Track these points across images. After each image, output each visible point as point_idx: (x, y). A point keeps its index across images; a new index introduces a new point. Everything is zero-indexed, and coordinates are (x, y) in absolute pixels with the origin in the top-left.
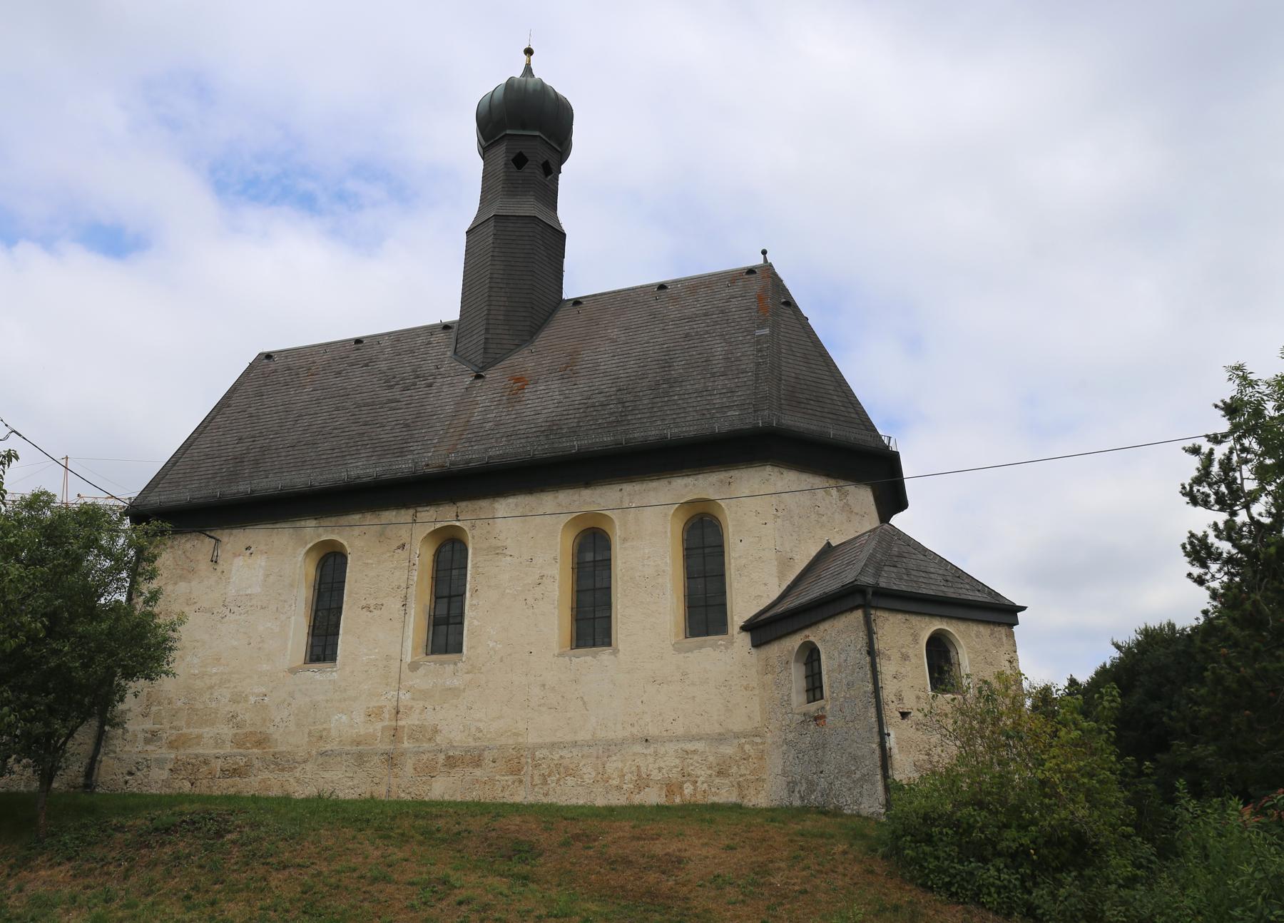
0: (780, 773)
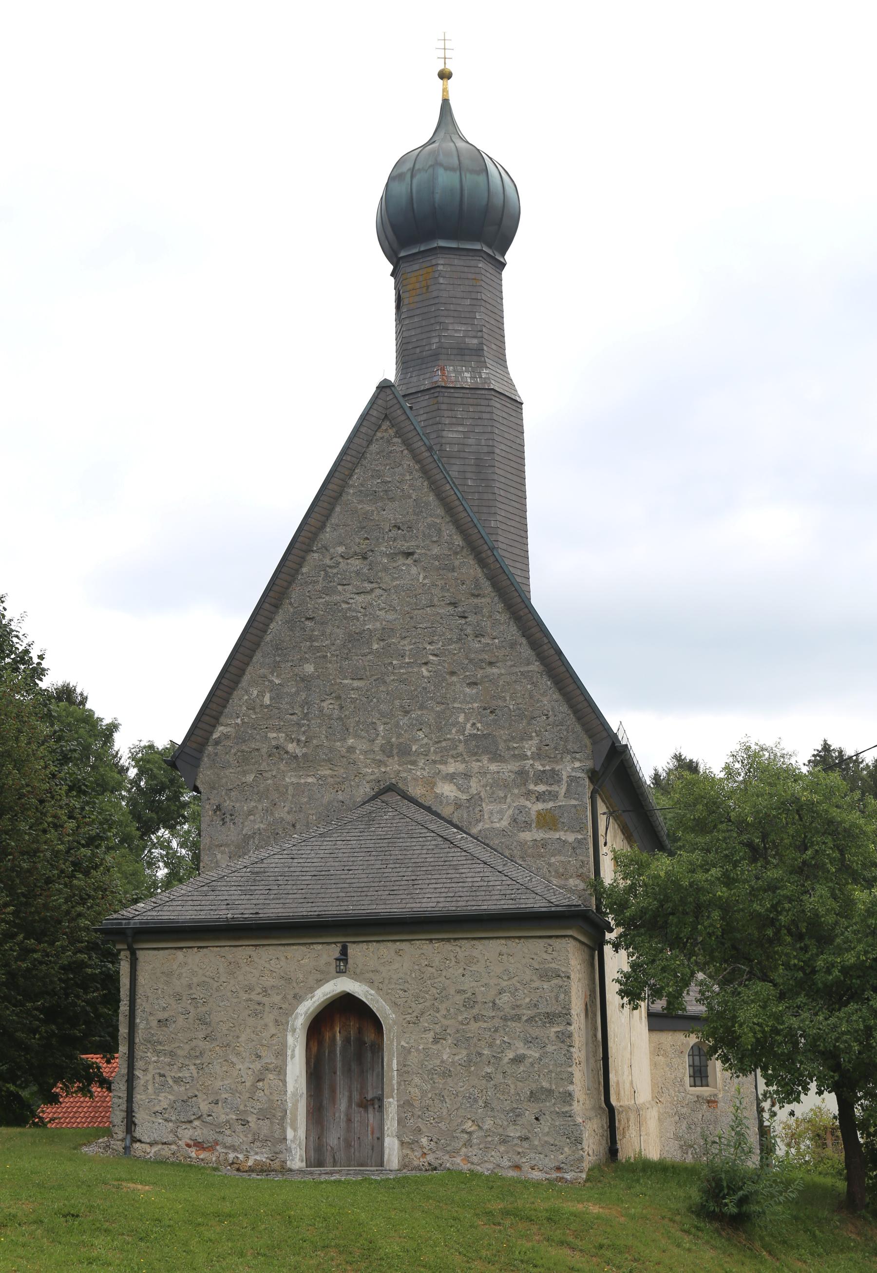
0: (672, 1137)
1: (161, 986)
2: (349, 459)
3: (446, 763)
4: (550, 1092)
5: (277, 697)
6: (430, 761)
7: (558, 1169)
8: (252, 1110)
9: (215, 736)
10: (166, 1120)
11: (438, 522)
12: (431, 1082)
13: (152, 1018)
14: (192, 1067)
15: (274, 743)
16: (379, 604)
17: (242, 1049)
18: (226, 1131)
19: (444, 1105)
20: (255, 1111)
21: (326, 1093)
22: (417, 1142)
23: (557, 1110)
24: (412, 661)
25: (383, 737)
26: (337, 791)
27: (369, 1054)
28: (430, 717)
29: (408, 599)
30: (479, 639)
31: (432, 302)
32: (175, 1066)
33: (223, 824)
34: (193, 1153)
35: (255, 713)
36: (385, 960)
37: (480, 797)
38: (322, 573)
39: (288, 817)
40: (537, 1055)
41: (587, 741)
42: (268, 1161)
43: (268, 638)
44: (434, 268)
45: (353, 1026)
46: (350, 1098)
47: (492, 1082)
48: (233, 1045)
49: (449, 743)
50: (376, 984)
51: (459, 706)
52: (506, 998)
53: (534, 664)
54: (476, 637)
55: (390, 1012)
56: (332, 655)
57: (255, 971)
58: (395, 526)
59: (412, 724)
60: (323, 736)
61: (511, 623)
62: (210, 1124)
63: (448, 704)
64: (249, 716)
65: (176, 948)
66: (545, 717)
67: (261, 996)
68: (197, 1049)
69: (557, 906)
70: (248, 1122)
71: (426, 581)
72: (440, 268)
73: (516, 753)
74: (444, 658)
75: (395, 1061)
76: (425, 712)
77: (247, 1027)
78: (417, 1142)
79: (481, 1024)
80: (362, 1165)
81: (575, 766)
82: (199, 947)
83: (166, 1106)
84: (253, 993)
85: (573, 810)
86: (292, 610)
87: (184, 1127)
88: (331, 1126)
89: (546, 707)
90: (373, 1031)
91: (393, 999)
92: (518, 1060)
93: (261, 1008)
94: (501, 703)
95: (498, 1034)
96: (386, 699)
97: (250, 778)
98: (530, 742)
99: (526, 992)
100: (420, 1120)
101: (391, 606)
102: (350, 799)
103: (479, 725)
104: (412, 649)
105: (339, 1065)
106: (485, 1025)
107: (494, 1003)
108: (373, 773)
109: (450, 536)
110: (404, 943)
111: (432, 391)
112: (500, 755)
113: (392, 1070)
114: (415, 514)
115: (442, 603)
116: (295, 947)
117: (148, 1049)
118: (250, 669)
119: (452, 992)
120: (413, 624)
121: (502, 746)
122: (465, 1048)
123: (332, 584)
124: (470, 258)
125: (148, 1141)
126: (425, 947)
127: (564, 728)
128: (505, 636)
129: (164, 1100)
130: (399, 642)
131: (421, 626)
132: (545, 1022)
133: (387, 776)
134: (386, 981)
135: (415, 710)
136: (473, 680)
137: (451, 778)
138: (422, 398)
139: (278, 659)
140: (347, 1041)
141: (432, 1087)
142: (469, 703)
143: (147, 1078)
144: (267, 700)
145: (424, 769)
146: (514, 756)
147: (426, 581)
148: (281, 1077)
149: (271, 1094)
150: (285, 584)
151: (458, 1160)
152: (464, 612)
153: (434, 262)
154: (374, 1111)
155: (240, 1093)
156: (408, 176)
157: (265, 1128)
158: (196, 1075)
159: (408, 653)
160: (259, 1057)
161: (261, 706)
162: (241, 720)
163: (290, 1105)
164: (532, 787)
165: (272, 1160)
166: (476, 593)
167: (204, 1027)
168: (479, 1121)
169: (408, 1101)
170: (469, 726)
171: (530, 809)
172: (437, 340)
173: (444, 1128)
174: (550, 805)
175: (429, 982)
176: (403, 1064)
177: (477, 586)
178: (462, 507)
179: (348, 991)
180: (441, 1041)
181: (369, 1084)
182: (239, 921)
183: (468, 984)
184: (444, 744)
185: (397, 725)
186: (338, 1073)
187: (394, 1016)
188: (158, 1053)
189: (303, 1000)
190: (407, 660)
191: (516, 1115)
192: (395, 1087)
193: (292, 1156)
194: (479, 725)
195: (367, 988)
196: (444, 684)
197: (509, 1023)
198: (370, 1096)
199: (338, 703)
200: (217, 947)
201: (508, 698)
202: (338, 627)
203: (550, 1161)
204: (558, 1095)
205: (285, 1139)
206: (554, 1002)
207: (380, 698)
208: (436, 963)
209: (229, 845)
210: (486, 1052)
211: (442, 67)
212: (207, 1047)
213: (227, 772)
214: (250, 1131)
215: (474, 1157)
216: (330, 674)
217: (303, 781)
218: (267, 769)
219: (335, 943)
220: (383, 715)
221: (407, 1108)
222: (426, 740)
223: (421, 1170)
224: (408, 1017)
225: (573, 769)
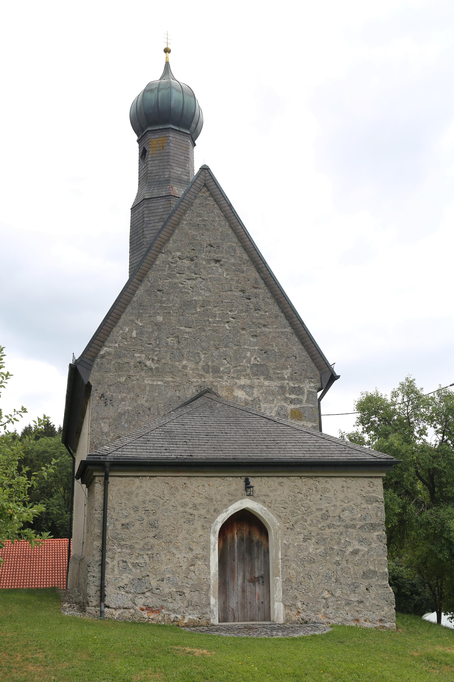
1: (124, 501)
2: (184, 205)
3: (240, 379)
4: (375, 572)
5: (140, 333)
6: (231, 377)
7: (381, 620)
8: (187, 585)
9: (102, 353)
10: (127, 592)
11: (234, 245)
12: (303, 566)
13: (118, 523)
14: (145, 556)
15: (138, 360)
16: (201, 287)
17: (180, 544)
18: (169, 600)
19: (311, 581)
20: (189, 586)
21: (229, 573)
22: (295, 605)
23: (379, 583)
24: (220, 320)
25: (204, 361)
26: (176, 391)
27: (256, 548)
28: (231, 352)
29: (217, 286)
30: (257, 312)
31: (166, 154)
32: (133, 556)
33: (105, 406)
34: (146, 615)
35: (127, 341)
36: (273, 488)
37: (259, 399)
38: (168, 265)
39: (146, 404)
40: (366, 550)
41: (318, 372)
42: (198, 619)
43: (135, 299)
44: (167, 138)
45: (245, 530)
46: (244, 577)
47: (340, 566)
48: (174, 542)
49: (242, 368)
50: (267, 503)
51: (247, 347)
52: (347, 514)
53: (288, 328)
54: (255, 310)
55: (276, 521)
56: (173, 312)
57: (188, 493)
58: (210, 245)
59: (220, 355)
60: (168, 358)
61: (275, 304)
62: (158, 595)
63: (241, 346)
64: (123, 343)
65: (134, 476)
66: (294, 358)
68: (149, 544)
69: (380, 458)
70: (184, 593)
71: (228, 277)
72: (170, 138)
73: (279, 376)
74: (238, 320)
75: (280, 553)
76: (228, 349)
77: (183, 530)
78: (295, 605)
79: (332, 530)
80: (252, 620)
81: (311, 386)
82: (150, 476)
83: (127, 583)
84: (187, 508)
85: (311, 410)
86: (149, 284)
87: (139, 597)
88: (232, 595)
89: (295, 352)
90: (258, 534)
91: (278, 513)
92: (355, 552)
93: (192, 517)
94: (270, 348)
95: (342, 536)
96: (205, 340)
97: (123, 379)
98: (287, 371)
99: (358, 510)
100: (296, 591)
101: (208, 288)
102: (184, 396)
103: (258, 359)
104: (220, 313)
105: (236, 555)
106: (334, 531)
107: (339, 517)
108: (197, 381)
109: (241, 254)
110: (284, 478)
111: (167, 197)
112: (270, 377)
113: (278, 559)
114: (221, 240)
115: (237, 290)
116: (214, 479)
117: (114, 544)
118: (123, 316)
119: (314, 509)
120: (221, 300)
121: (271, 371)
122: (323, 545)
123: (173, 272)
124: (185, 137)
125: (114, 607)
126: (297, 481)
127: (305, 364)
128: (272, 312)
129: (126, 578)
130: (213, 309)
131: (225, 301)
132: (370, 529)
133: (205, 384)
134: (274, 502)
135: (222, 348)
136: (255, 334)
137: (242, 387)
138: (161, 200)
139: (141, 311)
140: (241, 539)
141: (303, 570)
142: (252, 346)
143: (114, 564)
144: (134, 334)
145: (227, 382)
146: (278, 377)
147: (228, 277)
148: (207, 563)
149: (199, 574)
150: (146, 269)
151: (320, 616)
152: (249, 296)
153: (167, 135)
154: (259, 585)
155: (179, 574)
156: (156, 91)
157: (195, 597)
158: (148, 561)
159: (218, 315)
160: (191, 550)
161: (131, 337)
162: (118, 345)
163: (212, 581)
164: (288, 395)
165: (200, 619)
166: (256, 286)
167: (154, 529)
168: (333, 591)
169: (289, 578)
170: (253, 359)
171: (287, 408)
172: (168, 173)
173: (311, 596)
174: (298, 406)
175: (300, 503)
176: (285, 555)
177: (256, 282)
178: (248, 239)
179: (249, 507)
180: (308, 540)
182: (182, 460)
183: (324, 505)
184: (239, 368)
185: (212, 356)
186: (236, 560)
187: (279, 524)
188: (121, 546)
190: (217, 319)
191: (354, 587)
192: (281, 570)
193: (214, 616)
194: (258, 359)
196: (238, 335)
197: (349, 530)
198: (257, 575)
199: (176, 340)
200: (163, 476)
201: (274, 345)
202: (177, 297)
203: (377, 616)
204: (380, 574)
206: (375, 517)
207: (202, 339)
208: (304, 492)
209: (109, 418)
210: (335, 548)
211: (166, 47)
212: (156, 543)
213: (108, 375)
214: (185, 599)
215: (330, 614)
216: (172, 323)
217: (155, 383)
218: (133, 375)
219: (240, 477)
220: (203, 349)
222: (228, 365)
223: (297, 623)
224: (287, 525)
225: (310, 387)
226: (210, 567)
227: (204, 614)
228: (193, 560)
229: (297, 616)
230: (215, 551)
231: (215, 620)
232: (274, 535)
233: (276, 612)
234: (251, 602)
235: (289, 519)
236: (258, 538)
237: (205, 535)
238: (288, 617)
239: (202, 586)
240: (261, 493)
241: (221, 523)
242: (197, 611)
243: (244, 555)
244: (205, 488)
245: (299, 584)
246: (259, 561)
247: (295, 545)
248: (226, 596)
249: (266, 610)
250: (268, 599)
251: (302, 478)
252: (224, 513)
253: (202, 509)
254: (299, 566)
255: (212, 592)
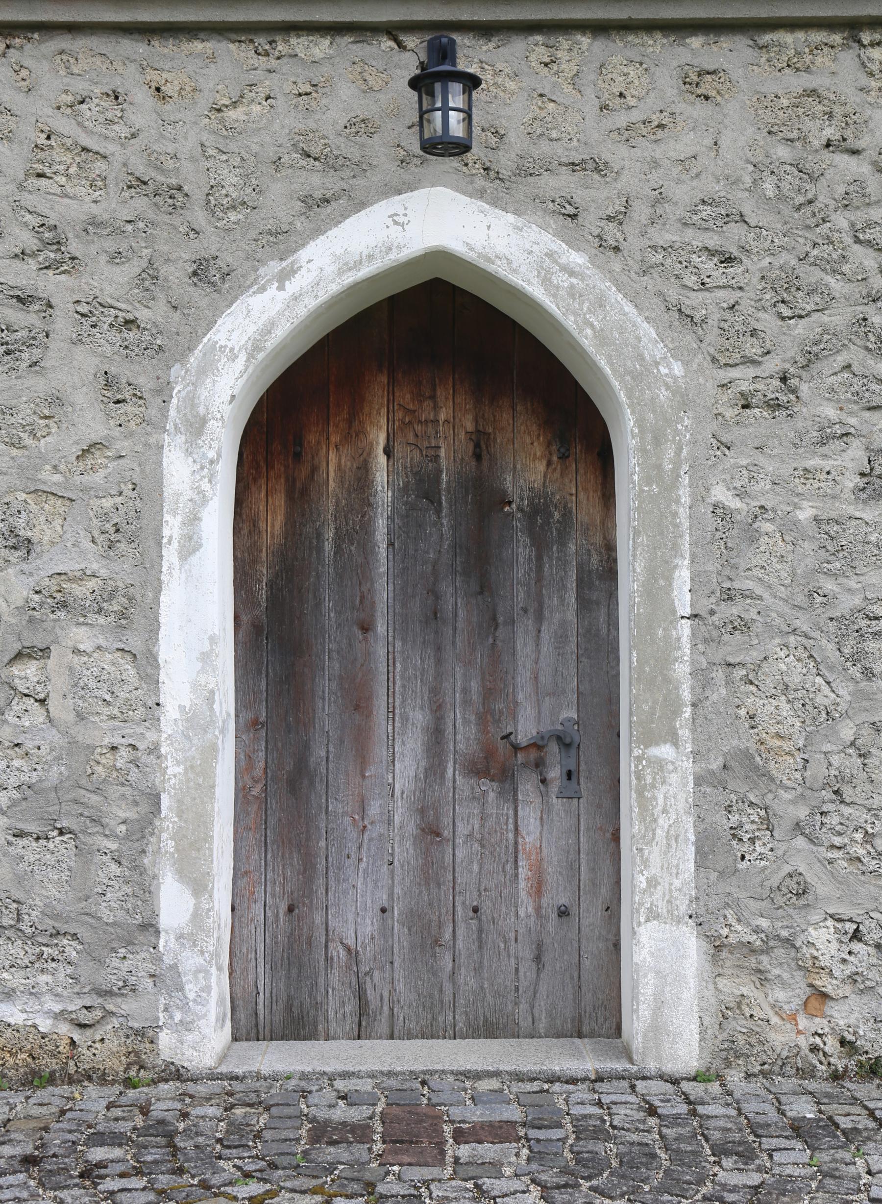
12: (855, 671)
22: (789, 943)
36: (636, 116)
42: (64, 1029)
50: (591, 221)
55: (659, 350)
67: (33, 264)
75: (683, 576)
78: (789, 943)
90: (538, 449)
91: (673, 293)
100: (800, 842)
110: (726, 42)
126: (822, 59)
134: (641, 212)
141: (859, 695)
148: (135, 642)
149: (81, 717)
163: (173, 769)
165: (82, 1026)
169: (746, 755)
175: (841, 220)
179: (457, 247)
181: (523, 677)
186: (381, 628)
187: (678, 369)
189: (242, 290)
192: (686, 695)
193: (184, 1007)
195: (548, 241)
205: (150, 927)
221: (743, 789)
226: (157, 667)
227: (109, 993)
228: (31, 620)
229: (803, 1022)
230: (194, 559)
231: (190, 1037)
232: (643, 450)
233: (647, 988)
234: (487, 909)
235: (754, 333)
236: (540, 478)
237: (123, 446)
238: (739, 1025)
239: (95, 799)
240: (545, 147)
241: (242, 358)
242: (61, 976)
243: (434, 593)
244: (129, 114)
245: (827, 794)
246: (545, 635)
247: (796, 523)
248: (308, 869)
249: (586, 963)
250: (604, 891)
251: (866, 37)
252: (263, 289)
253: (104, 258)
254: (831, 668)
255: (169, 845)
